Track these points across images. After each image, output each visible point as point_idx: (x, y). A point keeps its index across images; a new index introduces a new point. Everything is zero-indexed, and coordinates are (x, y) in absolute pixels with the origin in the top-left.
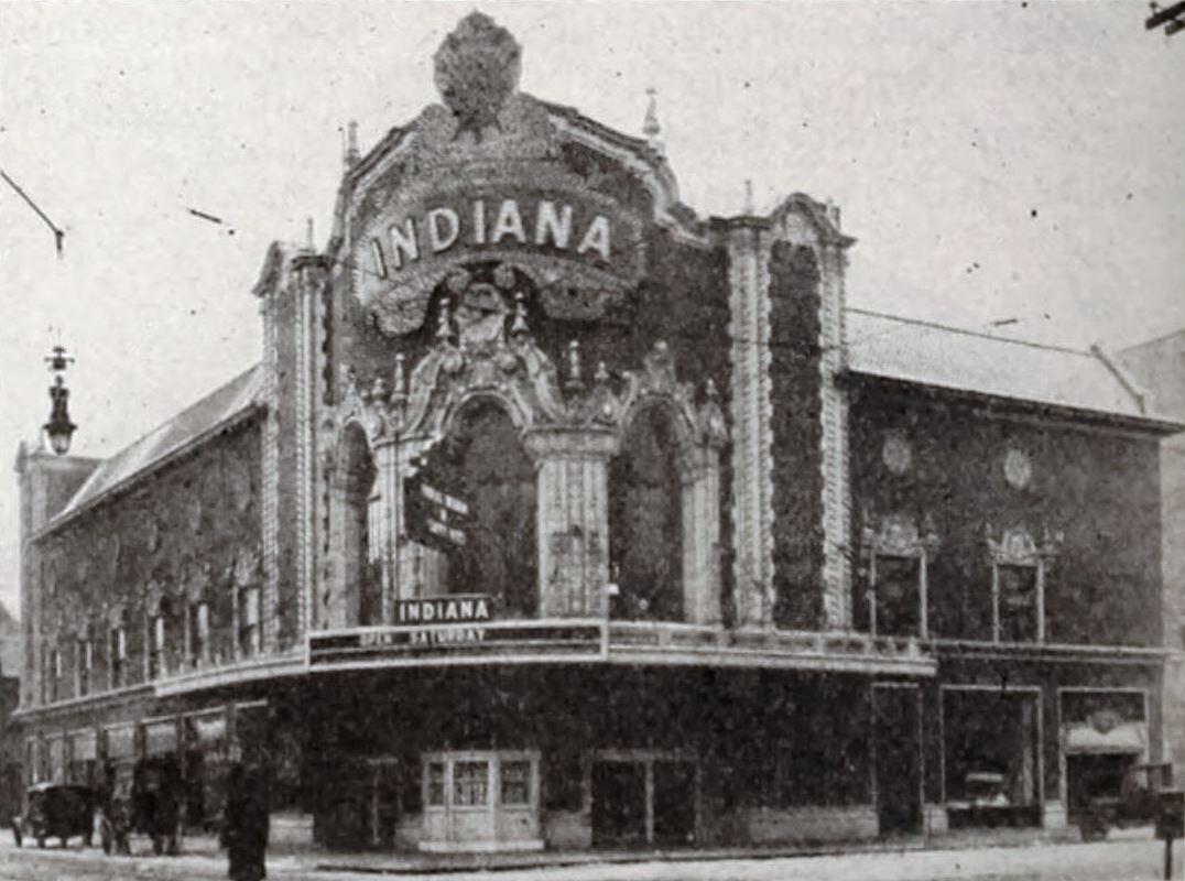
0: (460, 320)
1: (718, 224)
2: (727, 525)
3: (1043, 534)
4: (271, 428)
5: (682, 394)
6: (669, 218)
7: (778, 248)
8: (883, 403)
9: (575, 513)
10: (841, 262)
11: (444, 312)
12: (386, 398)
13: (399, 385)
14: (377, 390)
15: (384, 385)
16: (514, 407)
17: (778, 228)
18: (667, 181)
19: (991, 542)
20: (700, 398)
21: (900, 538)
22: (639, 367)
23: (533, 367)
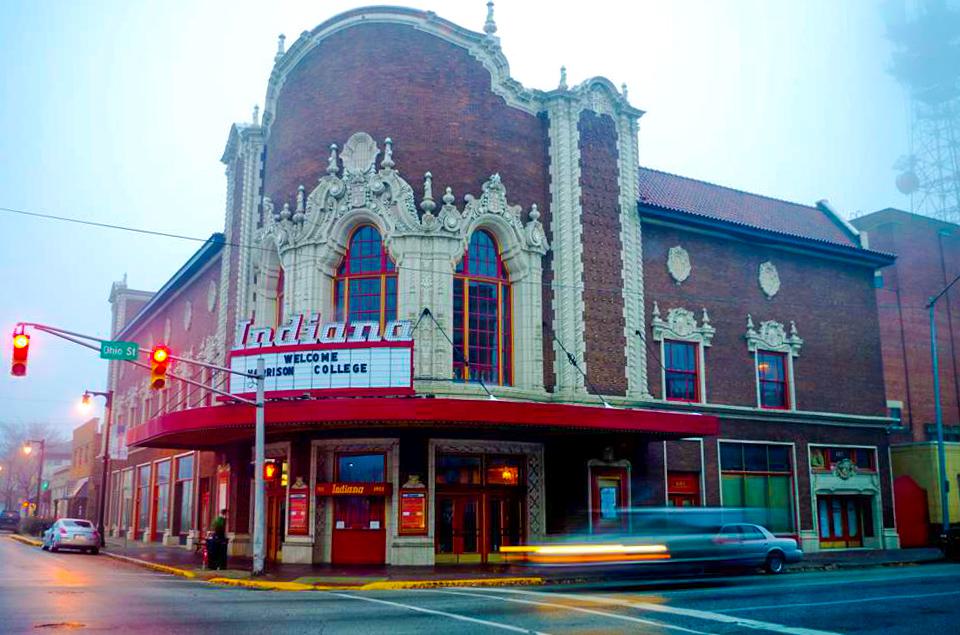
0: (344, 159)
1: (543, 97)
2: (548, 314)
3: (790, 329)
4: (226, 252)
5: (513, 213)
6: (502, 89)
7: (587, 114)
8: (666, 222)
9: (426, 299)
10: (633, 131)
11: (334, 153)
12: (290, 218)
13: (300, 207)
14: (285, 212)
15: (290, 209)
16: (381, 219)
17: (585, 101)
18: (502, 64)
19: (752, 333)
20: (526, 219)
21: (681, 325)
22: (478, 194)
23: (395, 190)
